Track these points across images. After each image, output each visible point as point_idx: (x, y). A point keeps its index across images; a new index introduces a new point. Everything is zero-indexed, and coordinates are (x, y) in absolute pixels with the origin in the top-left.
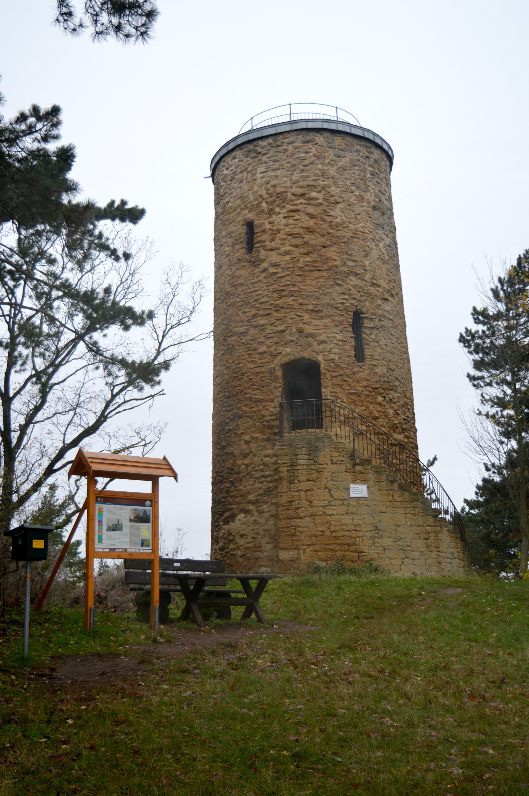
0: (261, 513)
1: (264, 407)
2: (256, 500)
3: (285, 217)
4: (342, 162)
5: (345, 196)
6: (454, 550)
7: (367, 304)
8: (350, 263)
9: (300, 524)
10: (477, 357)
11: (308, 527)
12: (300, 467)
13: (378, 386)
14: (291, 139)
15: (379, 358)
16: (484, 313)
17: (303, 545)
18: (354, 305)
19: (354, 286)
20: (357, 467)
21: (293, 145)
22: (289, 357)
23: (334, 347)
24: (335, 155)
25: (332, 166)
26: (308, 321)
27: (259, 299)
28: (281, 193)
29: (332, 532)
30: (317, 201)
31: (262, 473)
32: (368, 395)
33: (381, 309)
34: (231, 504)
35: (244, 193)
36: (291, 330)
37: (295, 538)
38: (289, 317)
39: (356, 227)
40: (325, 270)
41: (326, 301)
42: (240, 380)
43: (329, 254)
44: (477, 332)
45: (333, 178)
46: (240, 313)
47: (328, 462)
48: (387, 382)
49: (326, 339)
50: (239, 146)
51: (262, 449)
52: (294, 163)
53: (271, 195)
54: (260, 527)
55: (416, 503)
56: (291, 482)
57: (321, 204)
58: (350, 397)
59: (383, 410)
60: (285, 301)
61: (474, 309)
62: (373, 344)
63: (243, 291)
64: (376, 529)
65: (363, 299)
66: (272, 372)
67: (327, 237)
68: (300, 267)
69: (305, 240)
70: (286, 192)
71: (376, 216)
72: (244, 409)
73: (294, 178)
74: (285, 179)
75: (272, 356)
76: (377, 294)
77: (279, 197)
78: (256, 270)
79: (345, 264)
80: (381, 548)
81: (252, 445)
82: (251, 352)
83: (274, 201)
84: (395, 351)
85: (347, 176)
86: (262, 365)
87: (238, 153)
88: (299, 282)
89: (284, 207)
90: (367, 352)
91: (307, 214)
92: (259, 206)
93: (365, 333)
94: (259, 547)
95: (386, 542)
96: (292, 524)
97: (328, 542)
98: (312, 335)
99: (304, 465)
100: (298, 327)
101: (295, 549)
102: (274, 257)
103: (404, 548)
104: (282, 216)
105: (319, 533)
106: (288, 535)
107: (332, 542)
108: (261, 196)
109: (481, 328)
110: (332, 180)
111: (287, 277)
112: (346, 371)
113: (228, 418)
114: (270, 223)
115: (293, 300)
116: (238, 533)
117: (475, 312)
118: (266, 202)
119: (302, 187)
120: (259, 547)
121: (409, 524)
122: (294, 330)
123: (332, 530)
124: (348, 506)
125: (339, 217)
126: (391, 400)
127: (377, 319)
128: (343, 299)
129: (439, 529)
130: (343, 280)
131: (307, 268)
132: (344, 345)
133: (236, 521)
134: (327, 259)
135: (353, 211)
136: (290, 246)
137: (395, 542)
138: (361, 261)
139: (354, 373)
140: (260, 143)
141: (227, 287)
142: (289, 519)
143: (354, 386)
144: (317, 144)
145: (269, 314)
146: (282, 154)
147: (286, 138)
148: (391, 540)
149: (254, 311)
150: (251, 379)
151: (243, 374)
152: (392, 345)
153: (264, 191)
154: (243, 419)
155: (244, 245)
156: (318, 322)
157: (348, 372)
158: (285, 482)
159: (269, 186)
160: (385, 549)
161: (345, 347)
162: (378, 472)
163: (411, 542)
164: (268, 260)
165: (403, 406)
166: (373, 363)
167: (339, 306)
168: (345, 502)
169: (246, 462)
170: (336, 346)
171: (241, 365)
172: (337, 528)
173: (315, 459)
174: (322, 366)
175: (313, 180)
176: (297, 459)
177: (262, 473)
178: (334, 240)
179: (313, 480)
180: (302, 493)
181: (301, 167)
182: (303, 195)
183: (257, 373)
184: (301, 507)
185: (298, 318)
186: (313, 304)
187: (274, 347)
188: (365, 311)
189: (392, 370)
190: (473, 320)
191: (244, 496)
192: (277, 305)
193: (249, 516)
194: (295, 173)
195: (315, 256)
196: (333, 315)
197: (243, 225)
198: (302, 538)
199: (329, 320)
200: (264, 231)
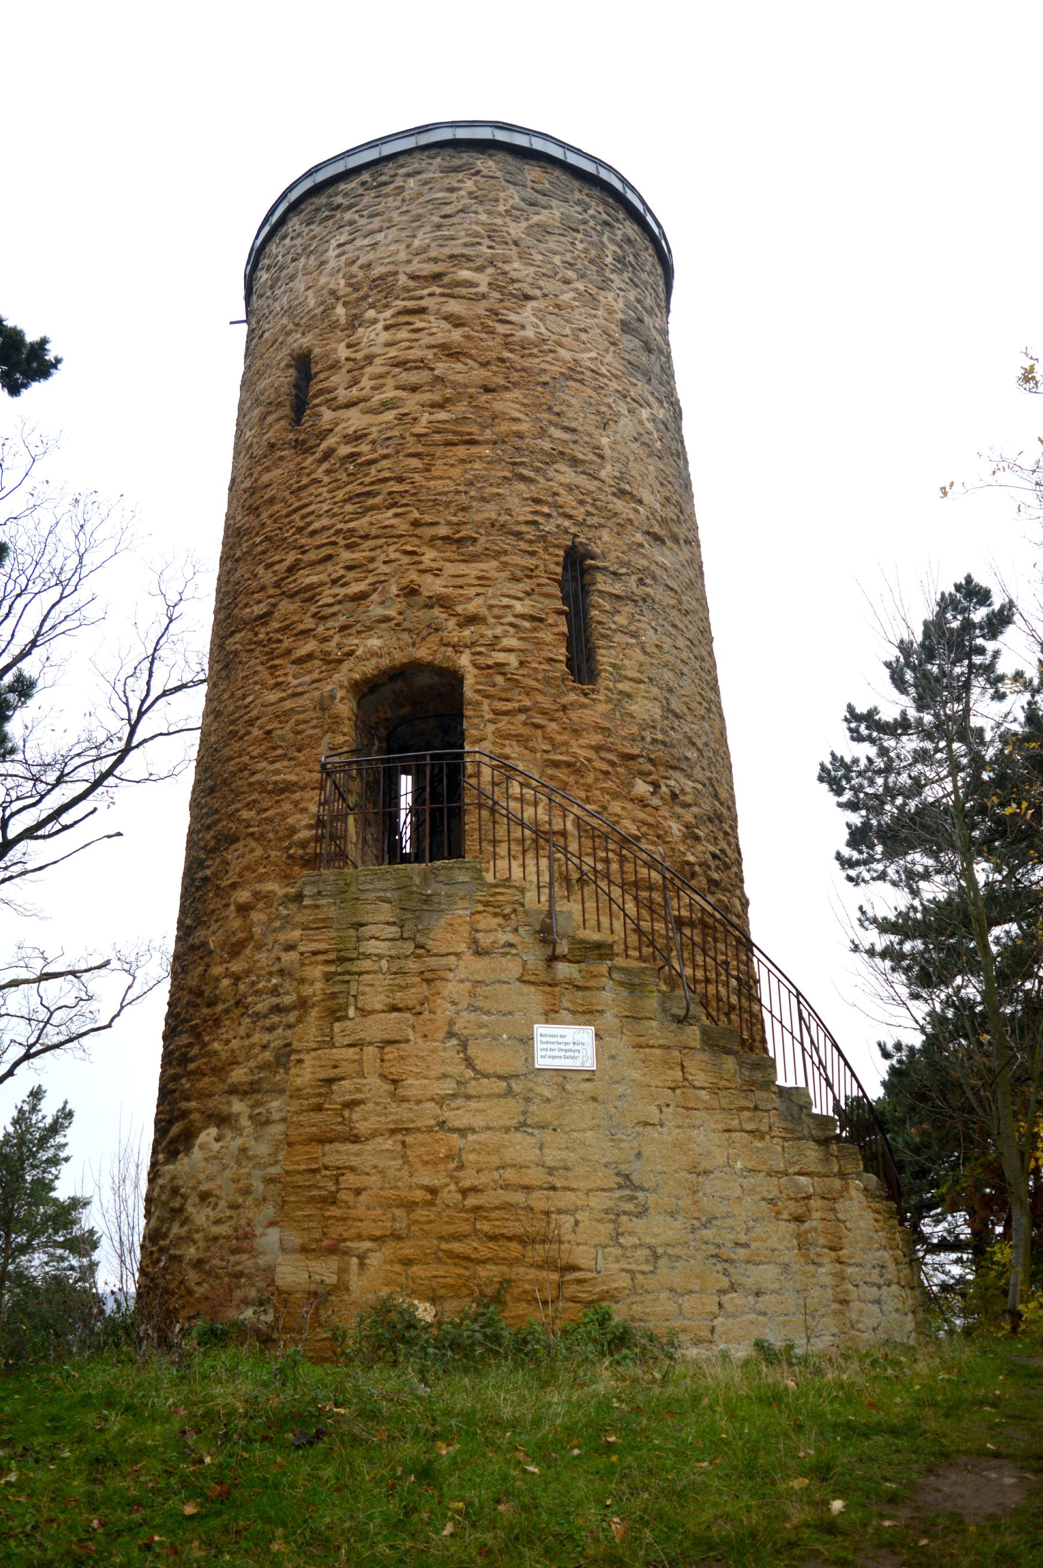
0: (261, 1122)
1: (296, 804)
2: (251, 1083)
3: (387, 328)
4: (542, 217)
5: (549, 286)
6: (886, 1255)
7: (606, 535)
8: (557, 433)
9: (354, 1162)
10: (856, 819)
11: (382, 1172)
12: (367, 964)
13: (636, 751)
14: (416, 165)
15: (637, 675)
16: (869, 718)
17: (360, 1237)
18: (566, 532)
19: (570, 488)
20: (562, 969)
21: (419, 177)
22: (374, 661)
23: (505, 634)
24: (523, 200)
25: (516, 219)
26: (435, 565)
27: (309, 524)
28: (382, 277)
29: (464, 1192)
30: (473, 290)
31: (275, 1000)
32: (606, 773)
33: (644, 556)
34: (187, 1099)
35: (297, 298)
36: (384, 591)
37: (334, 1211)
38: (383, 557)
39: (578, 356)
40: (486, 442)
41: (487, 515)
42: (241, 738)
43: (498, 406)
44: (856, 761)
45: (516, 243)
46: (260, 570)
47: (462, 947)
48: (664, 743)
49: (484, 611)
50: (294, 207)
51: (282, 927)
52: (419, 211)
53: (356, 287)
54: (257, 1172)
55: (759, 1094)
56: (336, 1014)
57: (484, 296)
58: (550, 772)
59: (650, 820)
60: (373, 520)
61: (850, 708)
62: (619, 637)
63: (271, 516)
64: (626, 1181)
65: (590, 521)
66: (323, 706)
67: (495, 368)
68: (419, 436)
69: (436, 372)
70: (397, 273)
71: (631, 346)
72: (245, 814)
73: (417, 243)
74: (393, 247)
75: (329, 662)
76: (632, 516)
77: (376, 286)
78: (310, 460)
79: (543, 433)
80: (642, 1253)
81: (256, 916)
82: (277, 662)
83: (365, 297)
84: (685, 670)
85: (552, 245)
86: (300, 690)
87: (294, 223)
88: (415, 470)
89: (387, 306)
90: (605, 657)
91: (445, 318)
92: (328, 316)
93: (598, 607)
94: (246, 1236)
95: (658, 1229)
96: (327, 1160)
97: (450, 1229)
98: (443, 602)
99: (380, 957)
100: (404, 582)
101: (332, 1250)
102: (355, 420)
103: (725, 1252)
104: (380, 326)
105: (419, 1195)
106: (312, 1199)
107: (465, 1228)
108: (333, 293)
109: (865, 751)
110: (514, 248)
111: (384, 462)
112: (540, 698)
113: (204, 848)
114: (349, 346)
115: (396, 515)
116: (194, 1188)
117: (853, 715)
118: (345, 304)
119: (435, 260)
120: (246, 1236)
121: (739, 1165)
122: (394, 590)
123: (467, 1183)
124: (528, 1100)
125: (529, 327)
126: (674, 796)
127: (634, 578)
128: (536, 513)
129: (837, 1183)
130: (538, 470)
131: (437, 437)
132: (535, 629)
133: (196, 1149)
134: (494, 417)
135: (567, 321)
136: (397, 388)
137: (693, 1230)
138: (590, 435)
139: (564, 708)
140: (343, 187)
141: (239, 518)
142: (321, 1141)
143: (565, 743)
144: (478, 173)
145: (329, 558)
146: (391, 199)
147: (402, 166)
148: (678, 1224)
149: (291, 558)
150: (269, 733)
151: (251, 723)
152: (674, 651)
153: (342, 282)
154: (239, 845)
155: (287, 411)
156: (461, 568)
157: (545, 702)
158: (314, 1013)
159: (355, 269)
160: (656, 1257)
161: (541, 635)
162: (633, 986)
163: (748, 1230)
164: (337, 430)
165: (710, 820)
166: (620, 686)
167: (524, 528)
168: (517, 1087)
169: (234, 969)
170: (512, 630)
171: (250, 699)
172: (484, 1179)
173: (421, 939)
174: (469, 682)
175: (466, 245)
176: (359, 939)
177: (275, 1000)
178: (515, 376)
179: (408, 1009)
180: (370, 1051)
181: (436, 219)
182: (437, 277)
183: (285, 713)
184: (361, 1102)
185: (406, 559)
186: (449, 523)
187: (337, 638)
188: (599, 551)
189: (677, 716)
190: (848, 734)
191: (220, 1071)
192: (352, 530)
193: (229, 1133)
194: (420, 234)
195: (461, 408)
196: (505, 553)
197: (288, 366)
198: (360, 1212)
199: (494, 563)
200: (335, 366)
